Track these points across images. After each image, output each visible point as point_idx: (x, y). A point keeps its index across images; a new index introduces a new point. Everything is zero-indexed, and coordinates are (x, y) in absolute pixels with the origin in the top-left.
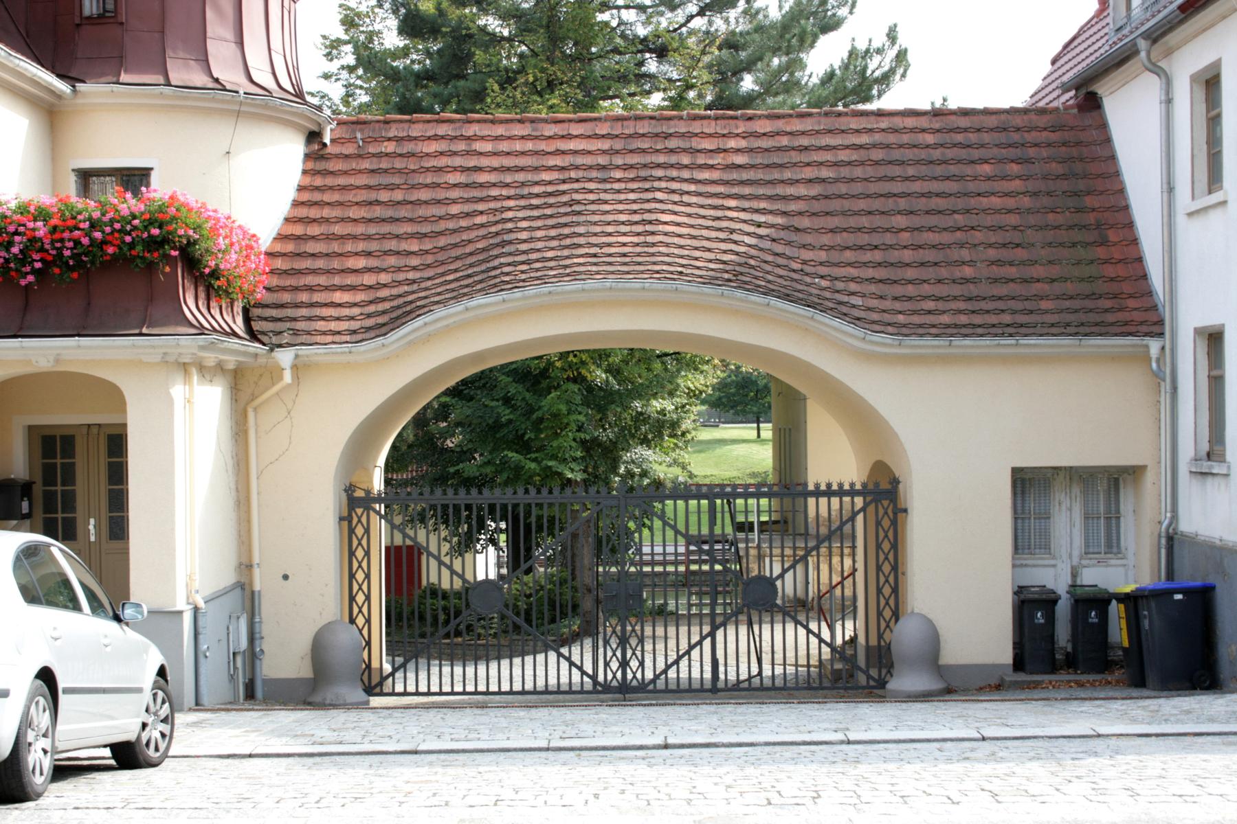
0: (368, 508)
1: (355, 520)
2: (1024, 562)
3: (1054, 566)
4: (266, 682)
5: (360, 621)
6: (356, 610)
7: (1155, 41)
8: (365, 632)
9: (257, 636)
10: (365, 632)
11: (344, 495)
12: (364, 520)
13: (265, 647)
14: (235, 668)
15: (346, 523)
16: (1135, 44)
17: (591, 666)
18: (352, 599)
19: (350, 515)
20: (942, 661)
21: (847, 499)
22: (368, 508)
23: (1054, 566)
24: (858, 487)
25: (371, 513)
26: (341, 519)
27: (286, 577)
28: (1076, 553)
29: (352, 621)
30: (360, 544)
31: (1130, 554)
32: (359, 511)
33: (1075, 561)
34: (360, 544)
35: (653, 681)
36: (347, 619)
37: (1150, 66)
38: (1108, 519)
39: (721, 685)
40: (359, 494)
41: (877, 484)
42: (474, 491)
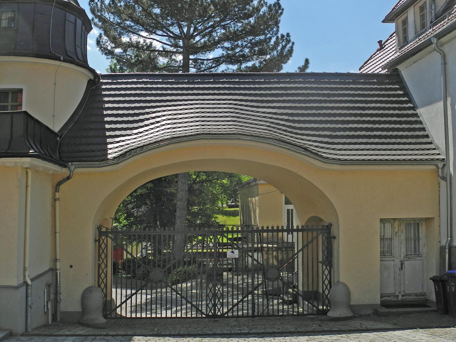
0: (107, 236)
1: (101, 241)
2: (386, 259)
3: (393, 260)
4: (62, 313)
5: (103, 286)
6: (101, 251)
7: (439, 39)
8: (104, 291)
9: (59, 292)
10: (104, 291)
11: (97, 230)
12: (105, 241)
13: (62, 297)
14: (47, 308)
15: (97, 243)
16: (431, 40)
17: (108, 242)
18: (99, 276)
19: (99, 239)
20: (352, 303)
21: (275, 234)
22: (107, 236)
23: (393, 260)
24: (300, 228)
25: (108, 238)
26: (96, 241)
27: (71, 266)
28: (402, 255)
29: (99, 286)
30: (103, 252)
31: (424, 256)
32: (103, 237)
33: (402, 258)
34: (103, 281)
35: (227, 313)
36: (97, 286)
37: (437, 49)
38: (415, 240)
39: (256, 314)
40: (104, 230)
41: (308, 226)
42: (152, 230)
